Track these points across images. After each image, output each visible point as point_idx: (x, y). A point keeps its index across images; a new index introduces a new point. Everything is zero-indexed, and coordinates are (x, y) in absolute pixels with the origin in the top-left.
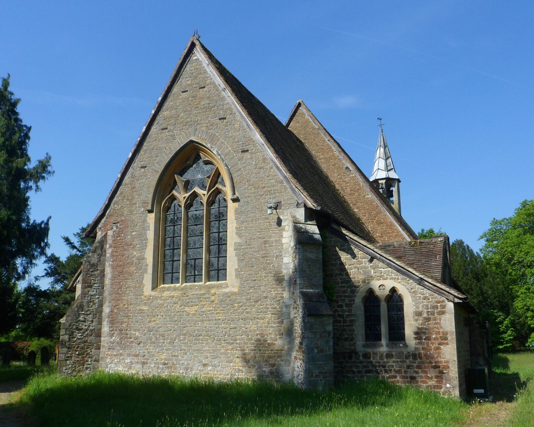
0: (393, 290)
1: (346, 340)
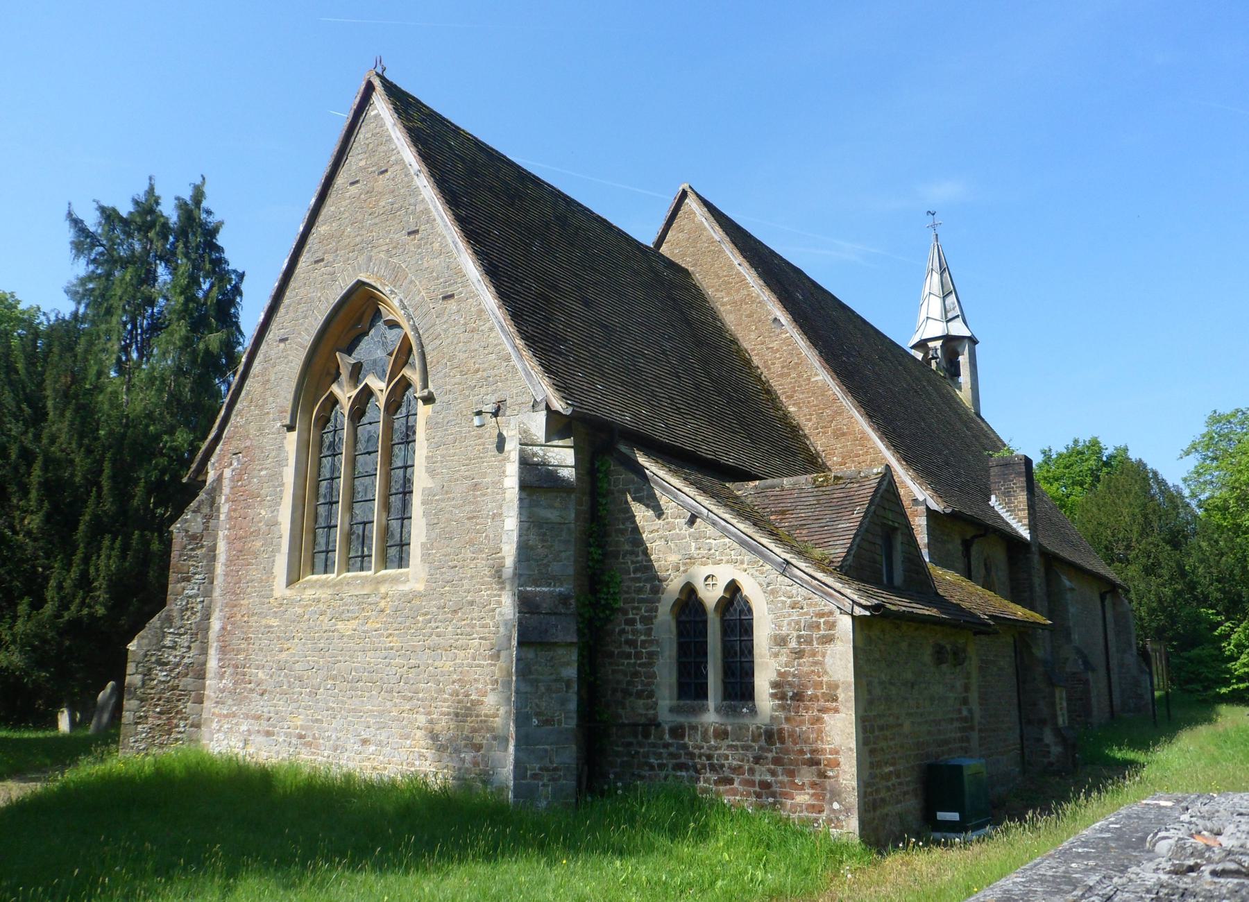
0: (733, 588)
1: (639, 695)
